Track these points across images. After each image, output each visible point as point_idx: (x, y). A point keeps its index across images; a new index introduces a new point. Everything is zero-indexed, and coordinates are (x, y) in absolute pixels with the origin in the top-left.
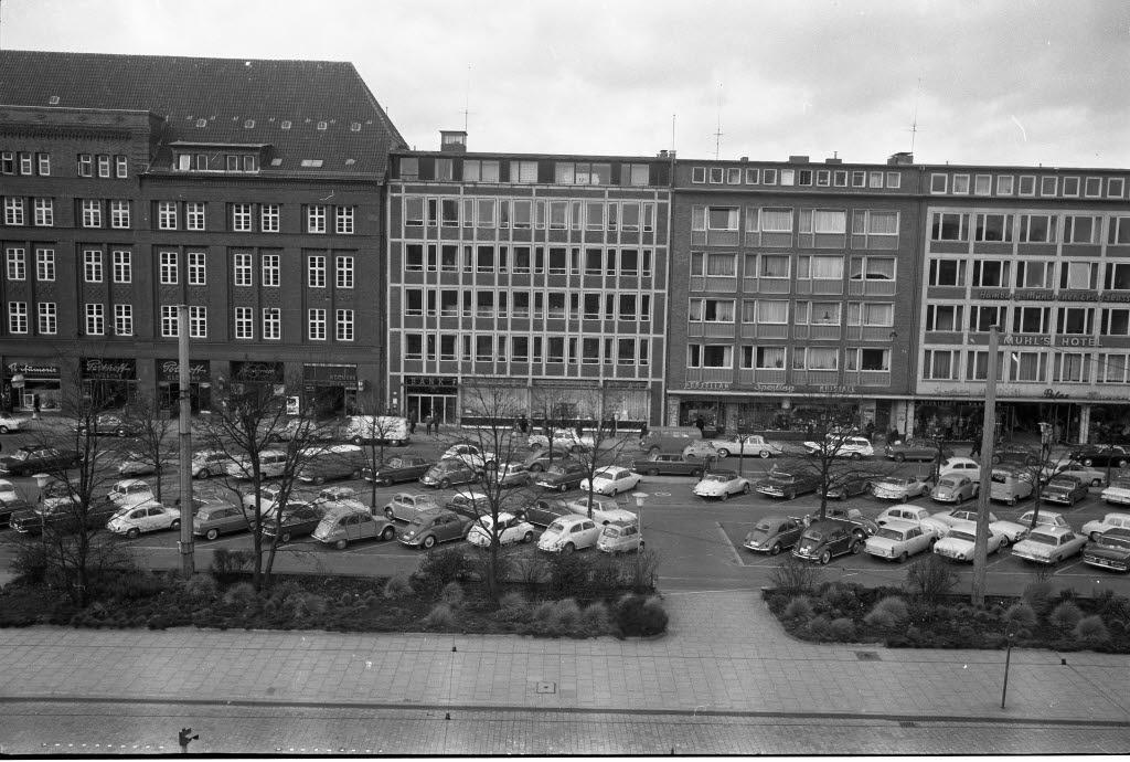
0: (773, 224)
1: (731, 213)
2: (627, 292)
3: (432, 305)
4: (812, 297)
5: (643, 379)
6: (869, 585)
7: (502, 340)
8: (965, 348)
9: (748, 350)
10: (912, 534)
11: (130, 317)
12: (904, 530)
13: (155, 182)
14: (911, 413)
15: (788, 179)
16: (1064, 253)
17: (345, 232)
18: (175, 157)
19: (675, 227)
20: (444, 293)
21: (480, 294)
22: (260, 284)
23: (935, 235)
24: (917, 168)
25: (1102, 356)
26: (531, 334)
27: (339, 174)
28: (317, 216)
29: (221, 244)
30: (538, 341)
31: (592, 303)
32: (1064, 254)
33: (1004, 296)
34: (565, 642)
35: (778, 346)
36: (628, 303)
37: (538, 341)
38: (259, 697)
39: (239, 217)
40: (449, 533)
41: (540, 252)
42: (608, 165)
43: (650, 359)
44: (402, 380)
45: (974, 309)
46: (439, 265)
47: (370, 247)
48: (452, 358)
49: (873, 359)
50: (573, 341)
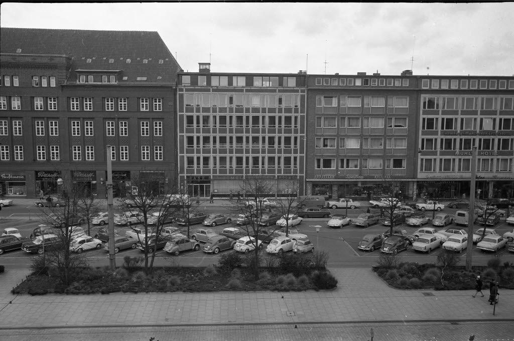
0: (352, 103)
1: (334, 99)
2: (287, 135)
3: (198, 143)
4: (370, 136)
5: (295, 175)
6: (421, 263)
7: (231, 158)
8: (438, 157)
9: (342, 161)
10: (432, 240)
11: (22, 151)
12: (429, 239)
13: (68, 89)
14: (415, 187)
15: (358, 83)
16: (481, 114)
17: (158, 110)
18: (78, 76)
19: (308, 104)
20: (253, 138)
21: (221, 138)
22: (49, 134)
23: (424, 107)
24: (416, 77)
25: (498, 159)
26: (244, 155)
27: (154, 84)
28: (145, 103)
29: (100, 117)
30: (247, 158)
31: (271, 140)
32: (461, 114)
33: (455, 134)
34: (28, 296)
35: (355, 158)
36: (288, 140)
37: (247, 158)
38: (162, 323)
39: (108, 104)
40: (226, 245)
41: (248, 118)
42: (278, 78)
43: (298, 166)
44: (185, 178)
45: (442, 140)
46: (201, 124)
47: (169, 117)
48: (208, 167)
49: (398, 163)
50: (263, 158)
